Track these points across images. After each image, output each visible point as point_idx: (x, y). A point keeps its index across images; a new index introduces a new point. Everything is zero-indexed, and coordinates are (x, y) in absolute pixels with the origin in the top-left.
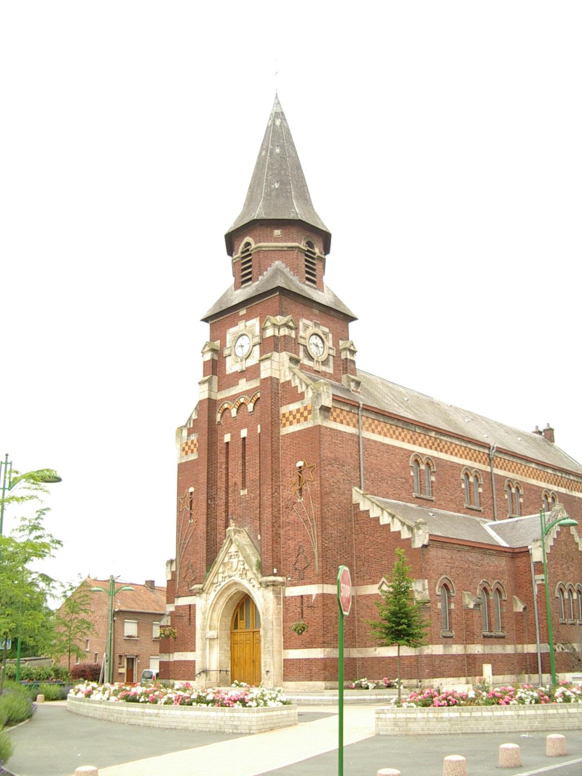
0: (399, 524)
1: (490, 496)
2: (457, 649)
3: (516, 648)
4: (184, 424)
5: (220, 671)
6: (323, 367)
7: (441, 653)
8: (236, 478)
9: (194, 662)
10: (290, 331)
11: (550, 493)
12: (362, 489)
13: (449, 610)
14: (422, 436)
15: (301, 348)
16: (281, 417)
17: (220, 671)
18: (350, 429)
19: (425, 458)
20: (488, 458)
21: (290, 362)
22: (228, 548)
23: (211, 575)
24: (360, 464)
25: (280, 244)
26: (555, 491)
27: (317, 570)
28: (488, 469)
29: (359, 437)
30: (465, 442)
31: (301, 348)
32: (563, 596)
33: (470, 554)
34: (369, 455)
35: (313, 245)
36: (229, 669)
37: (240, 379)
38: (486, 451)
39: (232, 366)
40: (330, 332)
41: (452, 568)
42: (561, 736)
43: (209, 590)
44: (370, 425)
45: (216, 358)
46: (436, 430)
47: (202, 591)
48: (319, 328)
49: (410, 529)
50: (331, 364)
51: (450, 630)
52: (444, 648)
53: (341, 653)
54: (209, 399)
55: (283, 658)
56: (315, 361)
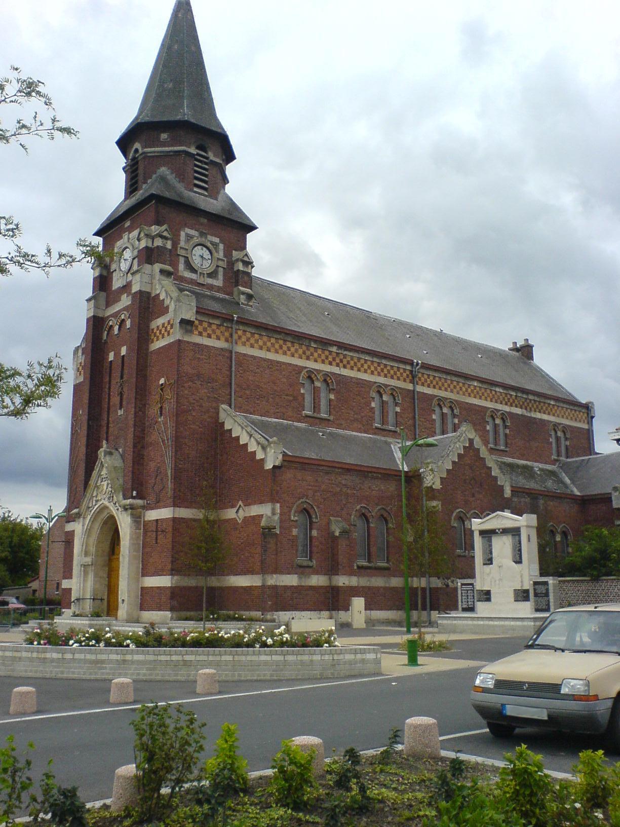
0: (255, 443)
1: (411, 415)
2: (317, 580)
4: (79, 345)
5: (94, 599)
6: (208, 279)
7: (295, 584)
8: (115, 400)
9: (70, 589)
10: (165, 241)
11: (499, 414)
12: (233, 407)
13: (310, 537)
14: (320, 351)
15: (182, 260)
16: (151, 331)
17: (94, 599)
18: (221, 344)
19: (321, 374)
20: (410, 375)
21: (161, 274)
22: (100, 471)
23: (86, 499)
24: (231, 380)
25: (167, 149)
26: (506, 412)
27: (170, 493)
28: (410, 387)
29: (231, 352)
30: (378, 358)
31: (182, 260)
32: (464, 526)
33: (345, 477)
34: (245, 371)
36: (105, 597)
37: (122, 294)
38: (408, 367)
39: (117, 282)
40: (220, 242)
41: (316, 491)
42: (212, 671)
43: (85, 514)
44: (248, 340)
45: (105, 273)
47: (78, 515)
48: (206, 238)
49: (264, 448)
50: (221, 276)
51: (311, 559)
52: (300, 578)
53: (264, 580)
54: (94, 316)
55: (140, 586)
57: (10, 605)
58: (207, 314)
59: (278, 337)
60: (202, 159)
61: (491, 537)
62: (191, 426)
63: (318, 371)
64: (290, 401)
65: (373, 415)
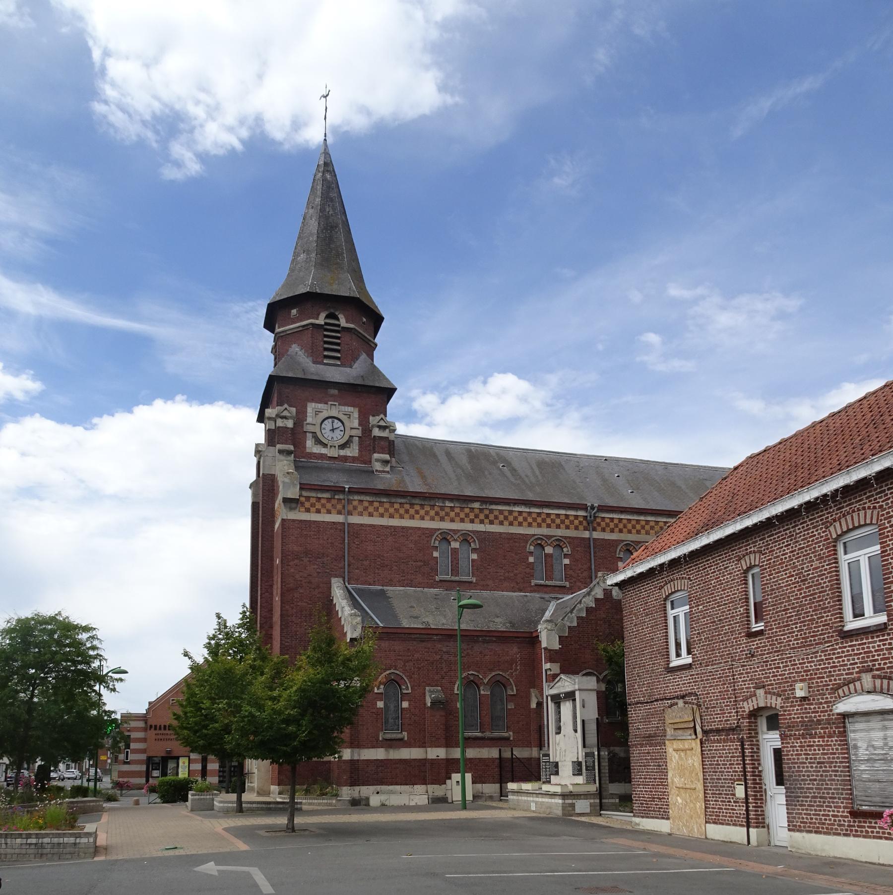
3: (359, 755)
35: (337, 316)
38: (581, 513)
44: (366, 509)
46: (480, 499)
56: (329, 446)
57: (580, 760)
58: (315, 489)
59: (403, 501)
60: (332, 328)
61: (560, 702)
62: (299, 604)
63: (455, 531)
64: (421, 567)
65: (532, 571)
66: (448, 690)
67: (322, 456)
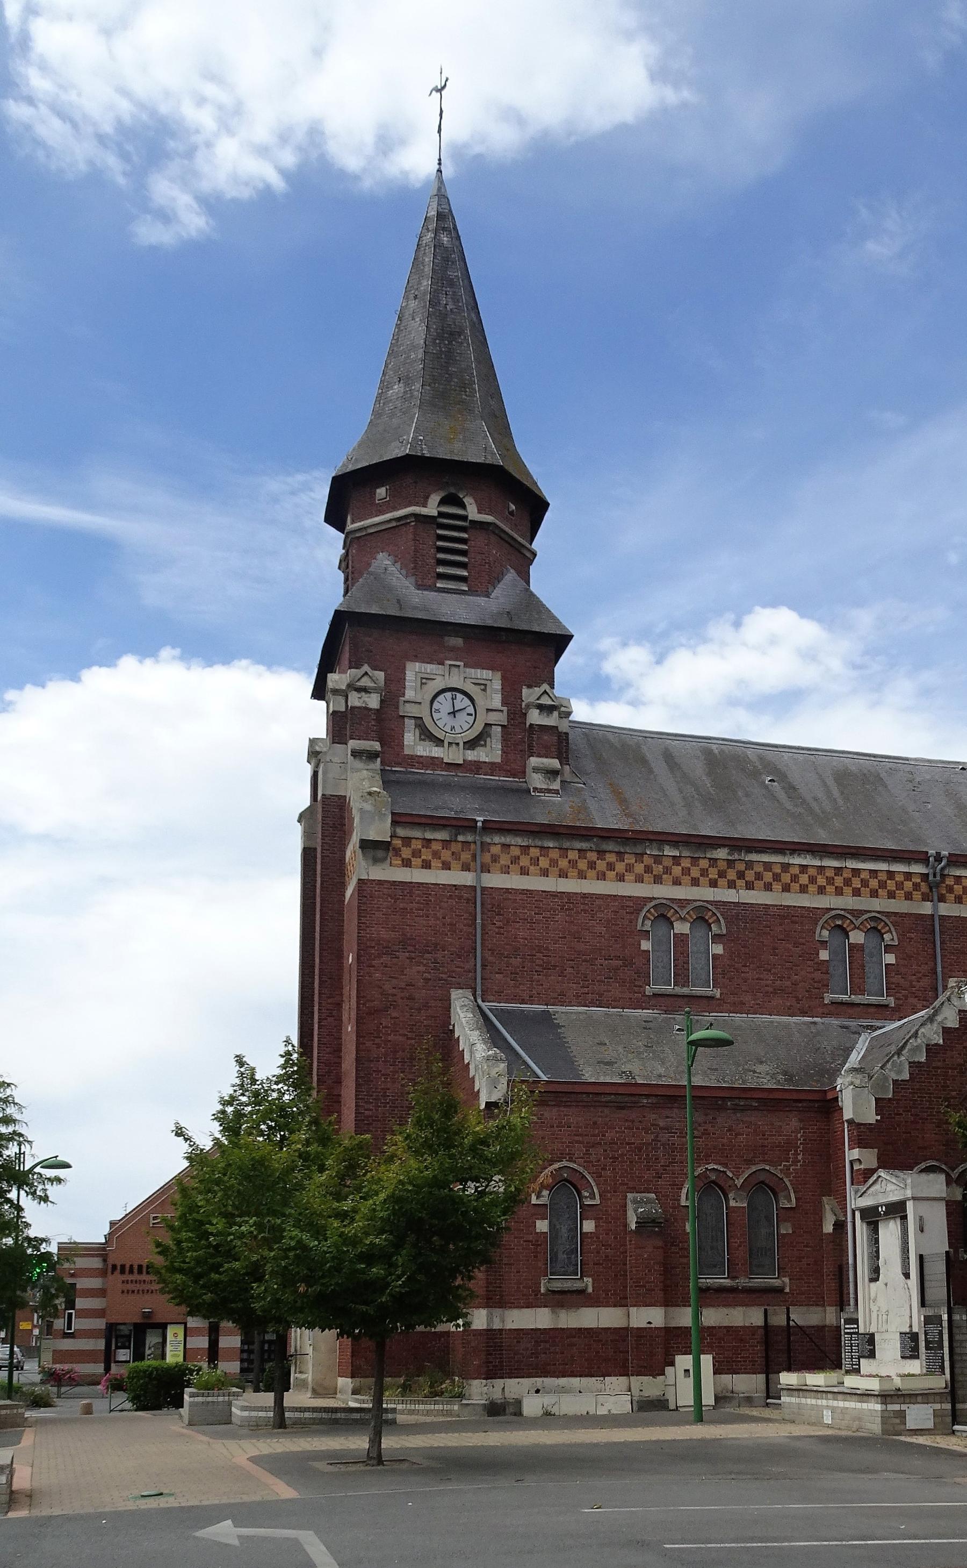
15: (409, 723)
44: (515, 860)
59: (584, 845)
64: (617, 969)
65: (825, 976)
66: (669, 1198)
67: (434, 762)
